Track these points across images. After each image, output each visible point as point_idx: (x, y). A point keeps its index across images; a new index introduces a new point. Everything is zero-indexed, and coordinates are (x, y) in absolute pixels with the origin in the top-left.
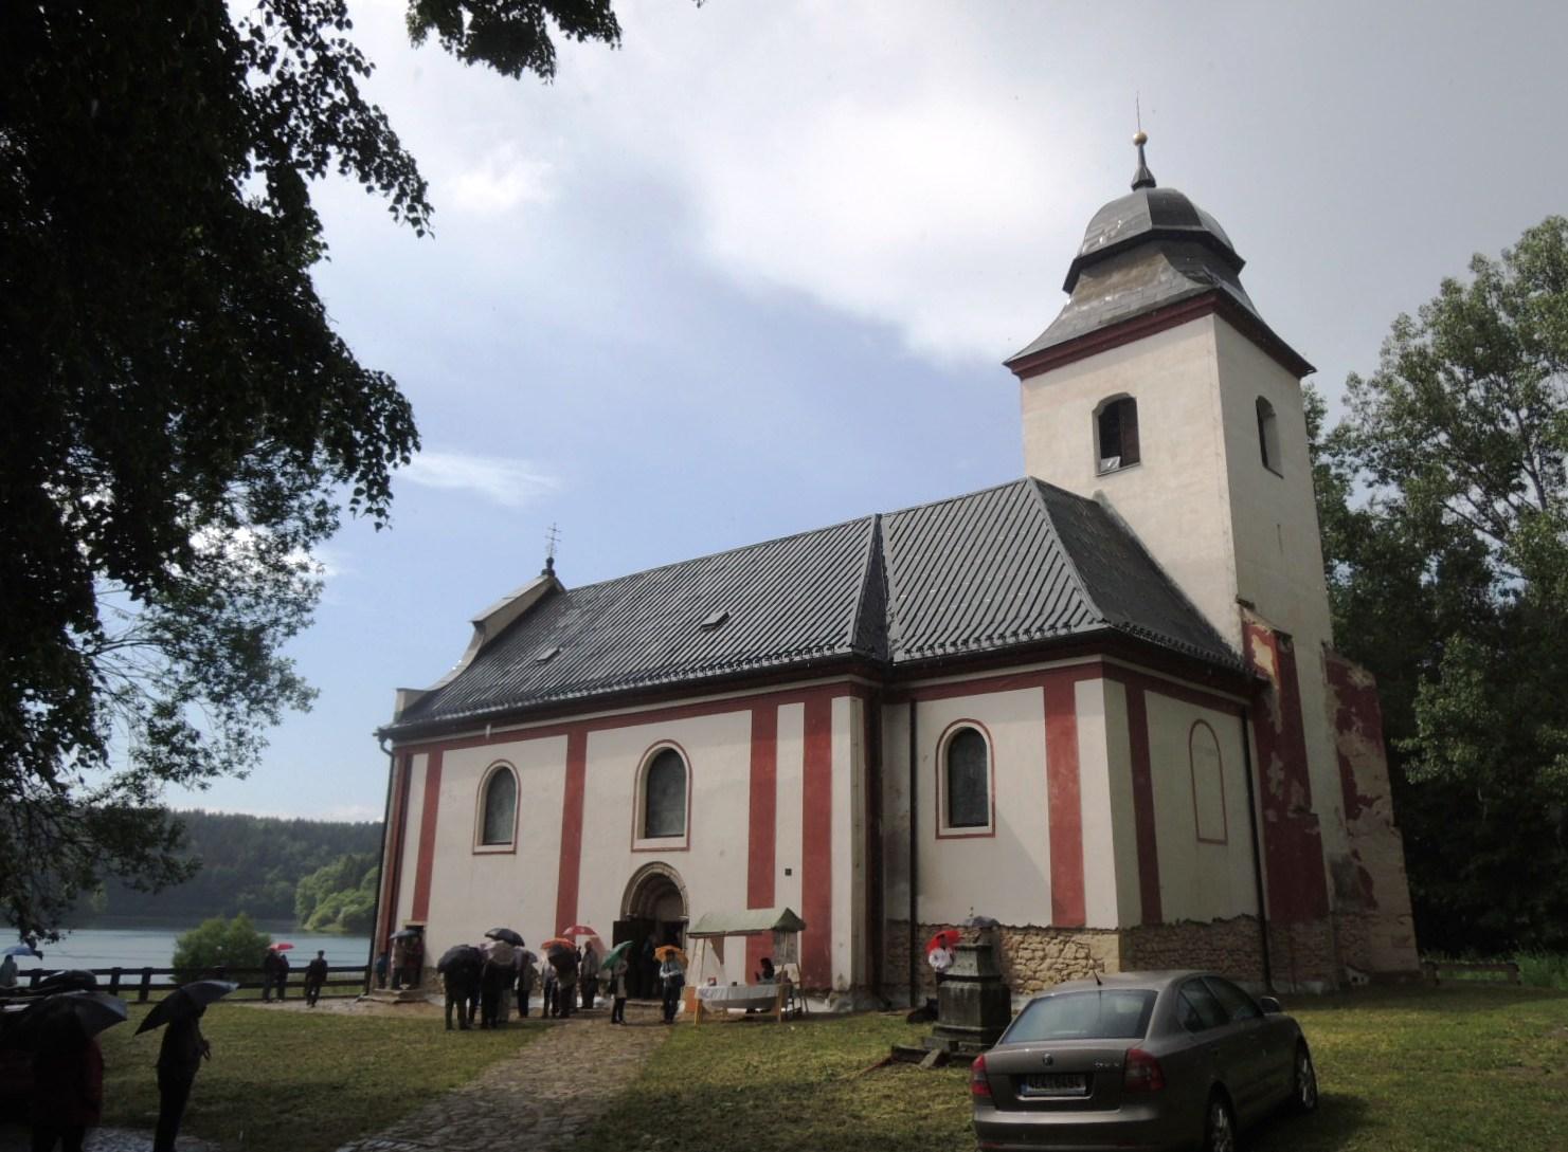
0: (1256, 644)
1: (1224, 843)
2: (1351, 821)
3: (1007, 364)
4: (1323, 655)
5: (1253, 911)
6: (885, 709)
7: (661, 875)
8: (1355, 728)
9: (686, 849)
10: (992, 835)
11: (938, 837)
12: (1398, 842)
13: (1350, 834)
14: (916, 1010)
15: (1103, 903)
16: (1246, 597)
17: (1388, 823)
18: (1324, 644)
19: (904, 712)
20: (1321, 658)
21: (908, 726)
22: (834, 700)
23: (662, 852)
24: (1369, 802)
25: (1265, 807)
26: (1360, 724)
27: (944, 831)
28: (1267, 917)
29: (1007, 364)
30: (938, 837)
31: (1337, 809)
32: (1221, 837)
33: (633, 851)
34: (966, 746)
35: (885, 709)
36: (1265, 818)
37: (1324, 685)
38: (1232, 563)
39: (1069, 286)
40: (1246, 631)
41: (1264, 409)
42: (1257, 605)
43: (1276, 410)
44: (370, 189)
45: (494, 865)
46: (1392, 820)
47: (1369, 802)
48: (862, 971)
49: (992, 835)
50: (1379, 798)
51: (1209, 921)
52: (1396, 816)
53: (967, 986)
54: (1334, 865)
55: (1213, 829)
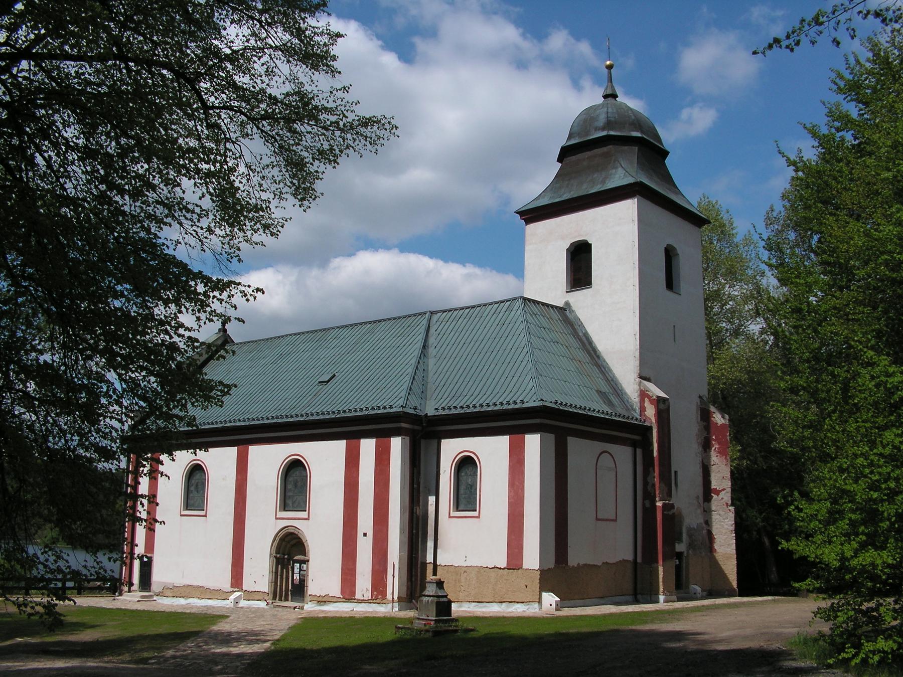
0: (647, 404)
1: (615, 520)
2: (706, 503)
3: (517, 212)
4: (699, 404)
5: (630, 557)
6: (423, 442)
7: (292, 534)
8: (713, 449)
9: (308, 519)
10: (478, 517)
11: (450, 517)
12: (732, 516)
13: (705, 511)
14: (135, 556)
15: (532, 558)
16: (644, 375)
17: (727, 504)
18: (700, 397)
19: (435, 442)
20: (697, 405)
21: (436, 451)
22: (392, 439)
23: (293, 520)
24: (718, 492)
25: (644, 499)
26: (717, 446)
27: (453, 514)
28: (639, 560)
29: (517, 212)
30: (450, 517)
31: (698, 497)
32: (614, 518)
33: (276, 519)
34: (466, 464)
35: (423, 442)
36: (644, 505)
37: (698, 422)
38: (637, 354)
39: (560, 160)
40: (643, 394)
41: (670, 254)
42: (652, 378)
43: (679, 251)
44: (234, 352)
45: (194, 523)
46: (730, 502)
47: (718, 492)
48: (405, 589)
49: (478, 517)
50: (724, 490)
51: (600, 564)
52: (732, 499)
53: (430, 599)
54: (690, 530)
55: (607, 511)
